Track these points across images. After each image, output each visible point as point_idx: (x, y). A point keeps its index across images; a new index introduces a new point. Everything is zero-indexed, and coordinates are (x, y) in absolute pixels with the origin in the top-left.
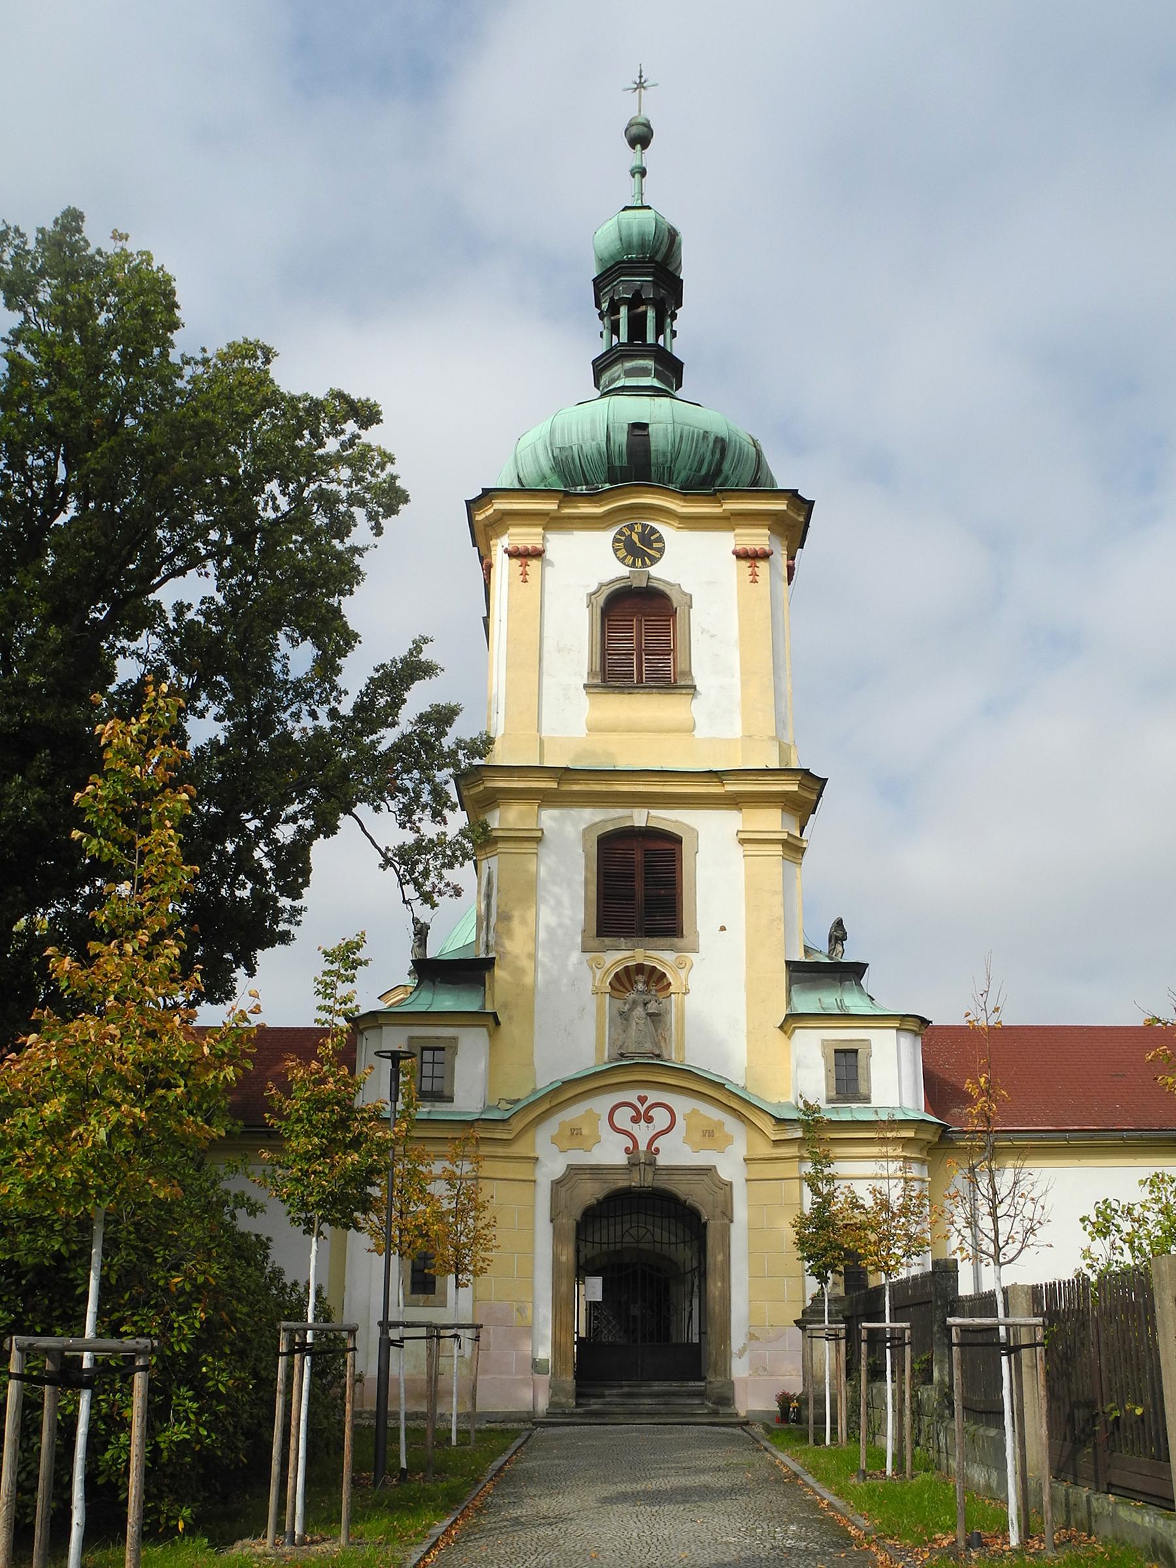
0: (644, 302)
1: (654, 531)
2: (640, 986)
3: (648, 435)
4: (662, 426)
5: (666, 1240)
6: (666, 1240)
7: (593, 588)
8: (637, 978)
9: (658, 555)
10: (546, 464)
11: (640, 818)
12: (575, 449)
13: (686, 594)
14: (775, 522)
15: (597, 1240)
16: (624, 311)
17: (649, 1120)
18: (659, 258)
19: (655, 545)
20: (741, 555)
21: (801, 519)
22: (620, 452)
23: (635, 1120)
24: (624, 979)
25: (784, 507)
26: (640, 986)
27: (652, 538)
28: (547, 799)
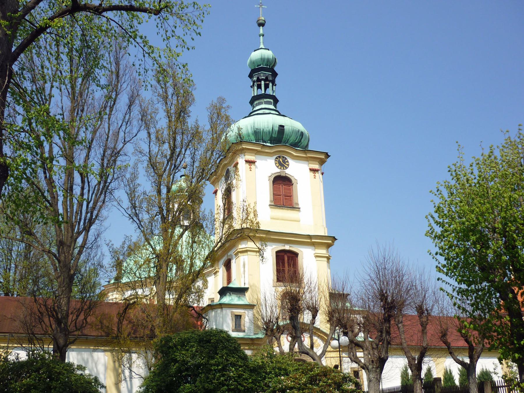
3: (284, 129)
4: (288, 127)
7: (270, 175)
10: (250, 131)
11: (287, 247)
12: (261, 130)
19: (286, 163)
20: (312, 170)
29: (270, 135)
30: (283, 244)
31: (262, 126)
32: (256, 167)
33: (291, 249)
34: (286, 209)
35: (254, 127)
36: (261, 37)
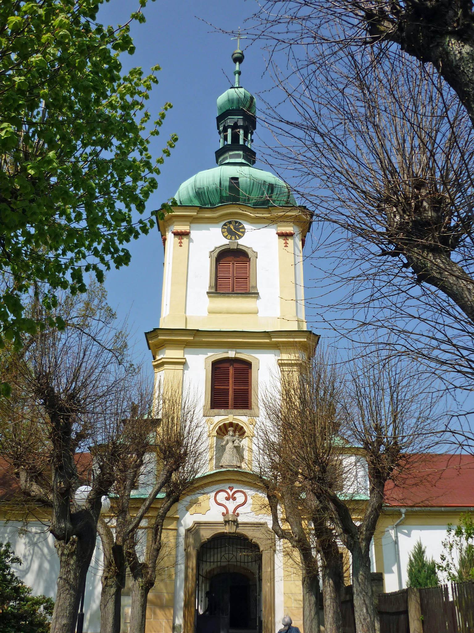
0: (240, 127)
1: (240, 224)
2: (231, 433)
3: (238, 183)
7: (212, 249)
8: (229, 429)
10: (191, 194)
11: (231, 354)
12: (205, 188)
13: (255, 252)
14: (296, 221)
15: (212, 560)
16: (229, 131)
17: (234, 499)
19: (241, 230)
20: (281, 235)
23: (227, 499)
24: (223, 430)
26: (231, 433)
28: (186, 345)
29: (219, 193)
30: (226, 350)
31: (205, 183)
33: (238, 356)
34: (234, 297)
35: (195, 186)
36: (237, 75)
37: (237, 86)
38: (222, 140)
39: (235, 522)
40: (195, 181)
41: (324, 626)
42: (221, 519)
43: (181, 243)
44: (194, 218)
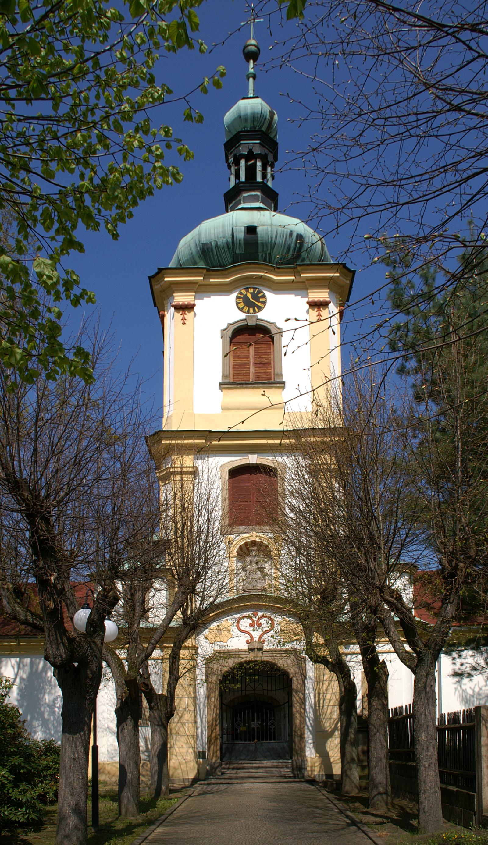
5: (269, 688)
6: (269, 688)
7: (224, 327)
9: (262, 306)
10: (194, 251)
11: (253, 459)
12: (213, 244)
16: (243, 162)
18: (264, 129)
19: (261, 300)
21: (348, 282)
22: (240, 245)
25: (338, 275)
27: (260, 295)
29: (231, 250)
31: (213, 236)
32: (195, 315)
36: (251, 80)
37: (252, 95)
38: (233, 178)
39: (260, 649)
40: (200, 234)
41: (417, 646)
42: (245, 647)
43: (184, 319)
44: (200, 285)
